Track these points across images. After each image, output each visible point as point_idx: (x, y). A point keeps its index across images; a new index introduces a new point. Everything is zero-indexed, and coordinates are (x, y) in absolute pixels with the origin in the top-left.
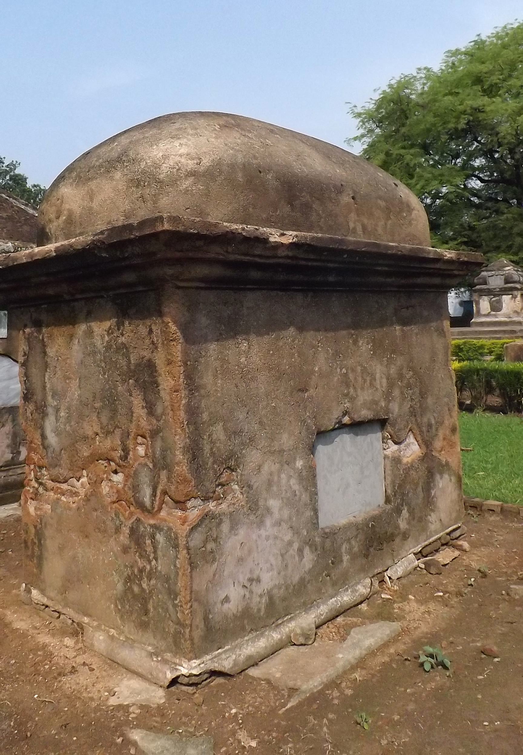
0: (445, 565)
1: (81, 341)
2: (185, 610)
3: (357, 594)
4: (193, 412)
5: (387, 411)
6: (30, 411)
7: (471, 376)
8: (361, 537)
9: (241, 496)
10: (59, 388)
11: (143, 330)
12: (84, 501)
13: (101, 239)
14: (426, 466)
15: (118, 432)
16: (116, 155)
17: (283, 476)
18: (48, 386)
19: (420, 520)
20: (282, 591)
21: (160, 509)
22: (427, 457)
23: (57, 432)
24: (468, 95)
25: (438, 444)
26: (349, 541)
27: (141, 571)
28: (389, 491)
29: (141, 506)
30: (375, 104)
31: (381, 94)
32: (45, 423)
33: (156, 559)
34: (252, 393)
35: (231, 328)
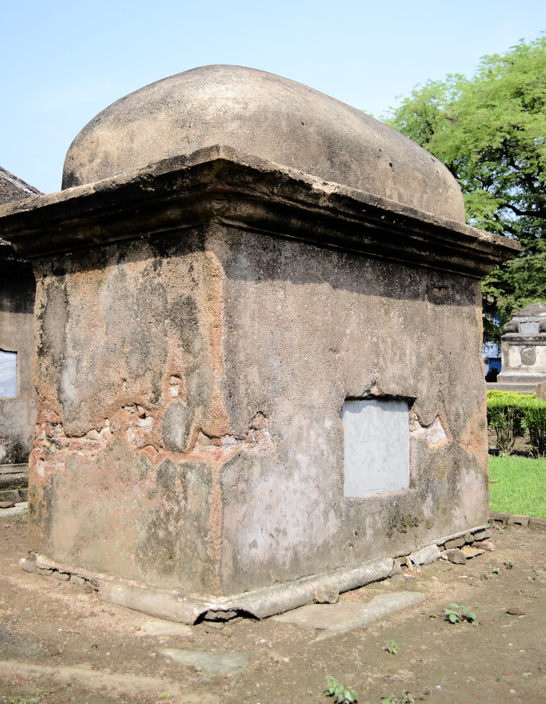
0: (469, 558)
1: (110, 285)
2: (215, 546)
3: (380, 570)
4: (231, 350)
5: (416, 391)
6: (45, 365)
7: (498, 413)
8: (385, 514)
9: (271, 444)
10: (82, 338)
11: (183, 268)
12: (106, 451)
13: (150, 172)
14: (453, 456)
15: (149, 376)
16: (160, 97)
17: (312, 433)
18: (69, 336)
19: (445, 511)
20: (306, 550)
21: (193, 447)
22: (453, 447)
23: (77, 384)
24: (506, 110)
25: (465, 436)
26: (373, 515)
27: (167, 514)
28: (414, 475)
29: (173, 448)
30: (396, 114)
31: (403, 102)
32: (63, 376)
33: (186, 499)
34: (286, 343)
35: (269, 271)
